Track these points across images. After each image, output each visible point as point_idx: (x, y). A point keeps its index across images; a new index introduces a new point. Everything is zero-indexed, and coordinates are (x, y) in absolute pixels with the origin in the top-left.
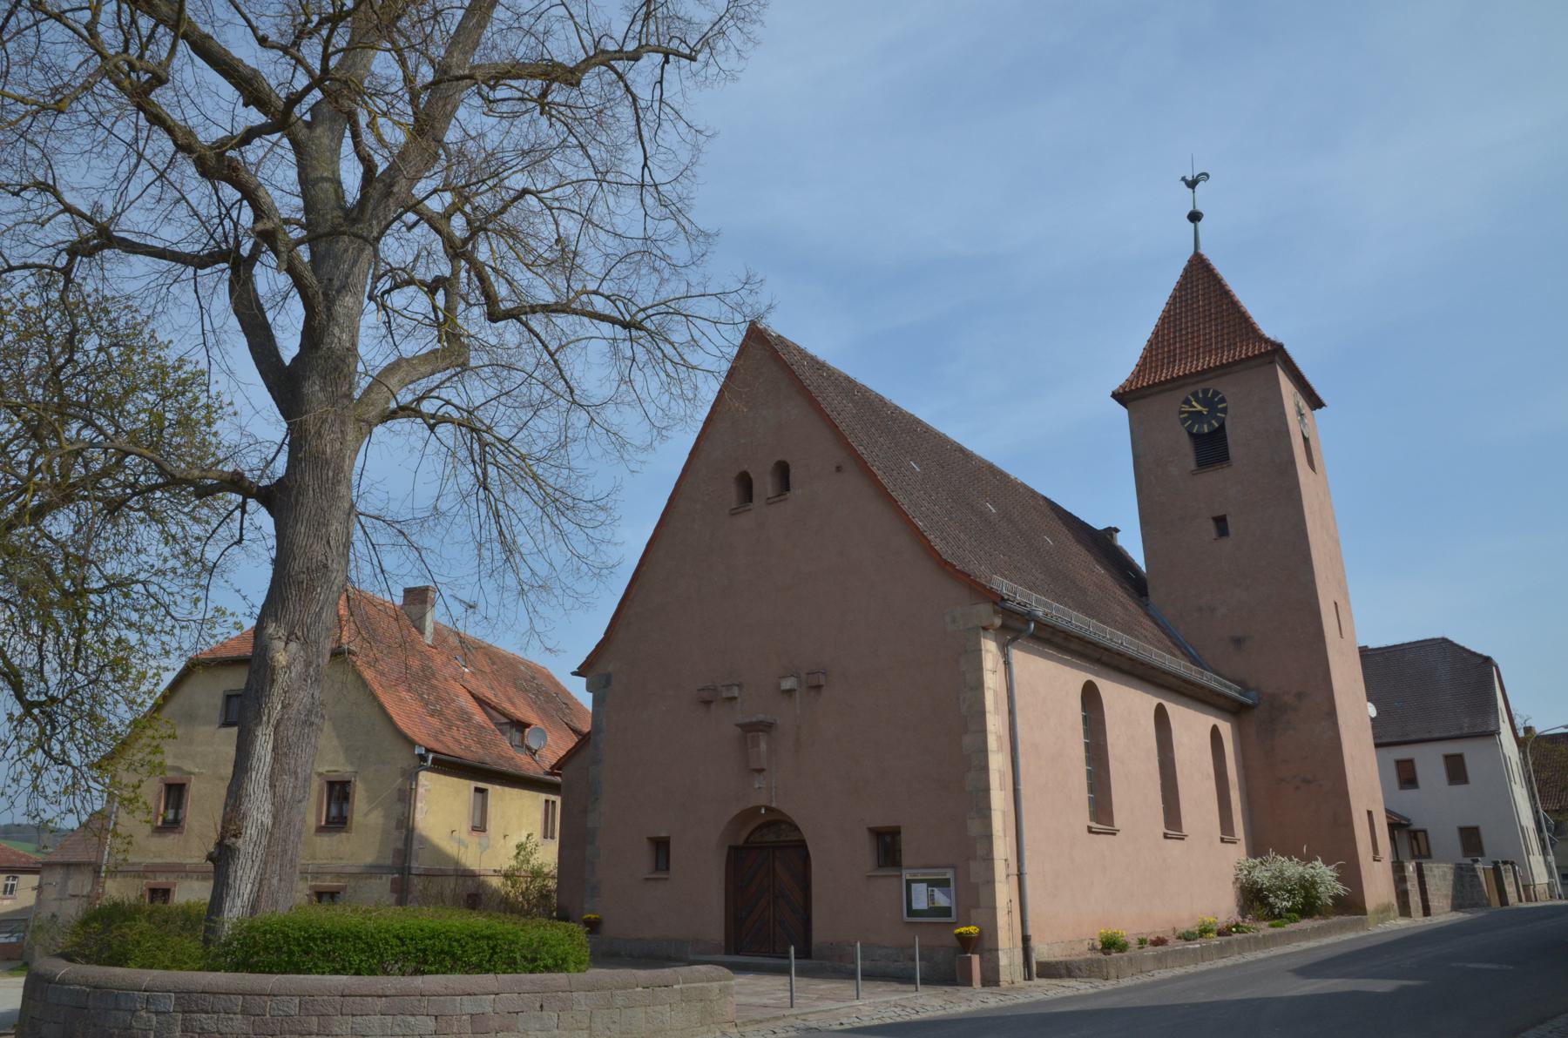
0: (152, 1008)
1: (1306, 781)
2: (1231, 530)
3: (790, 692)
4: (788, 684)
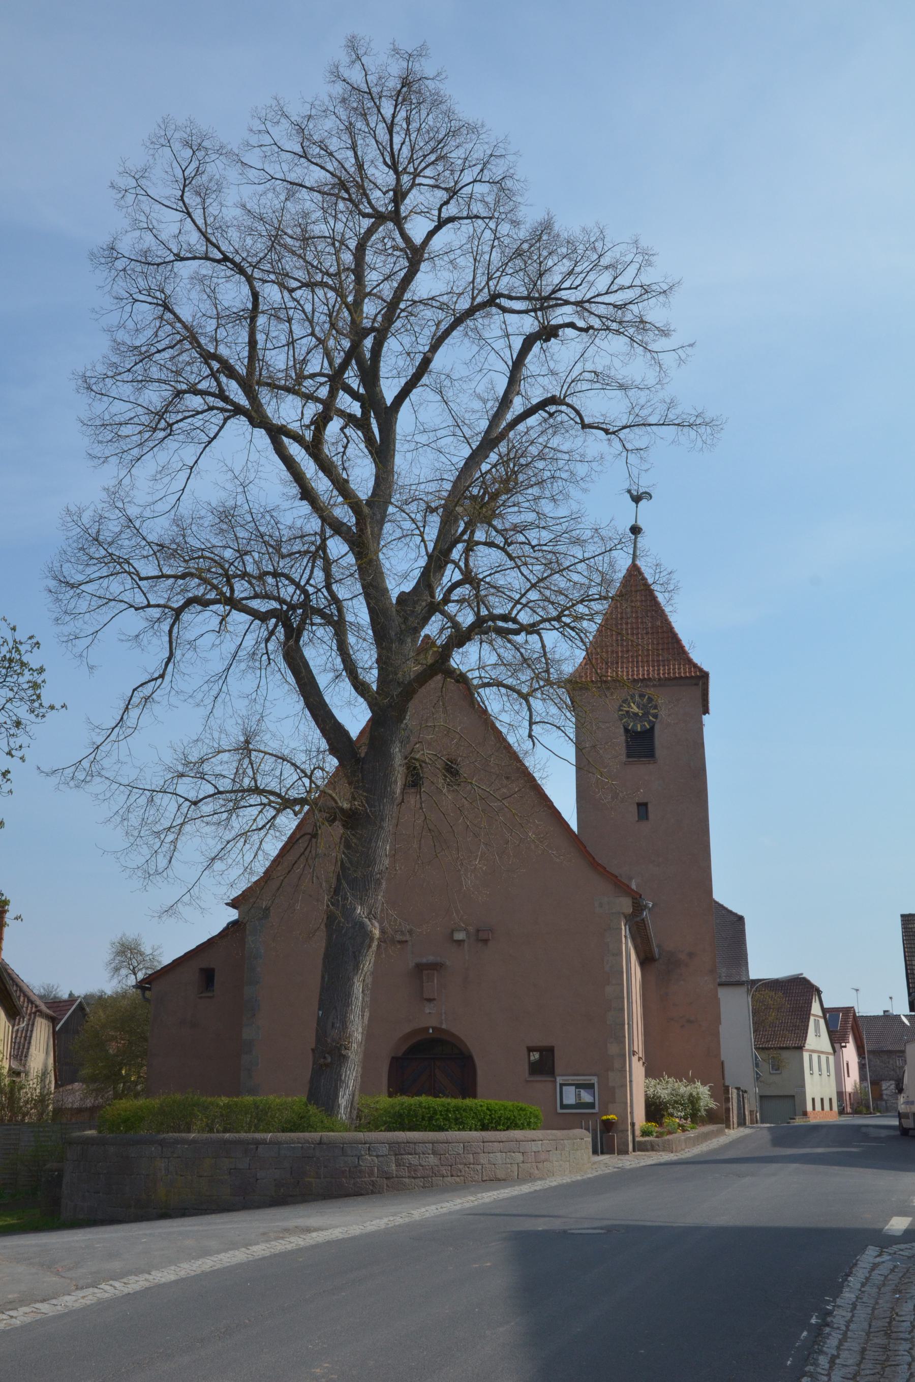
0: (375, 1154)
2: (651, 816)
3: (459, 942)
4: (459, 936)
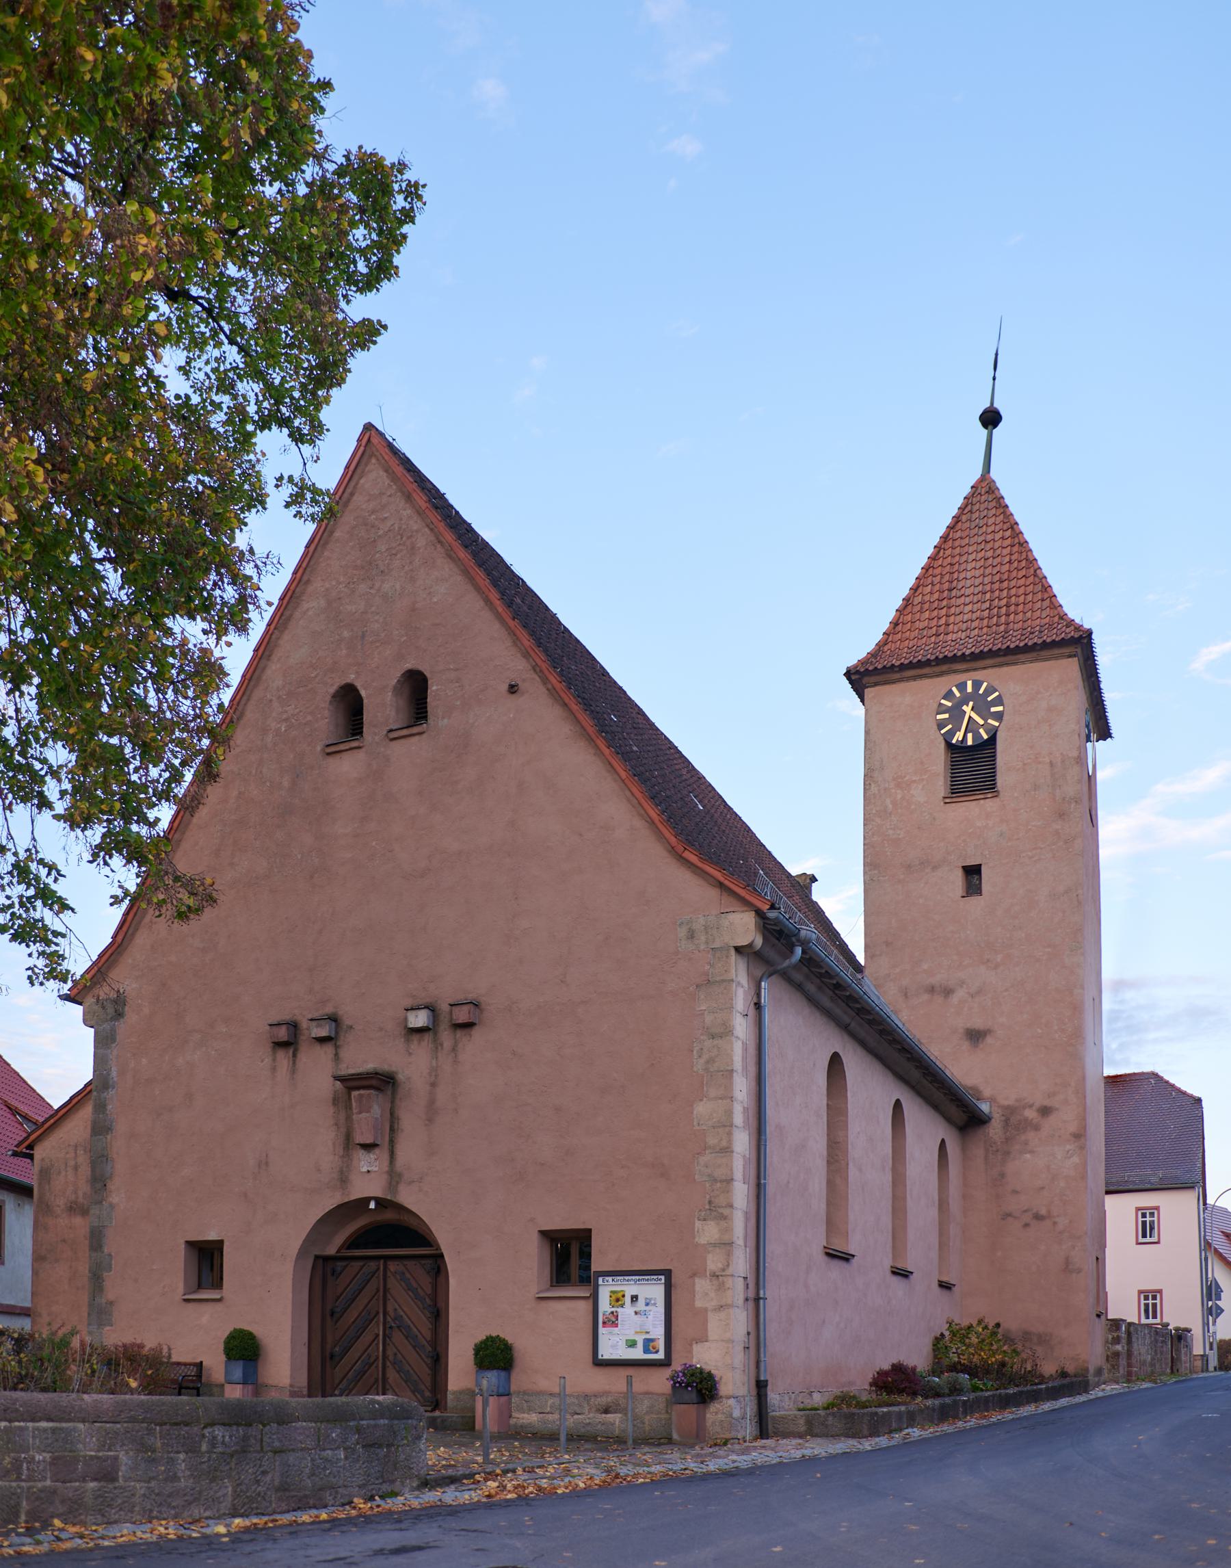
1: (1038, 1217)
2: (985, 887)
4: (419, 1019)
